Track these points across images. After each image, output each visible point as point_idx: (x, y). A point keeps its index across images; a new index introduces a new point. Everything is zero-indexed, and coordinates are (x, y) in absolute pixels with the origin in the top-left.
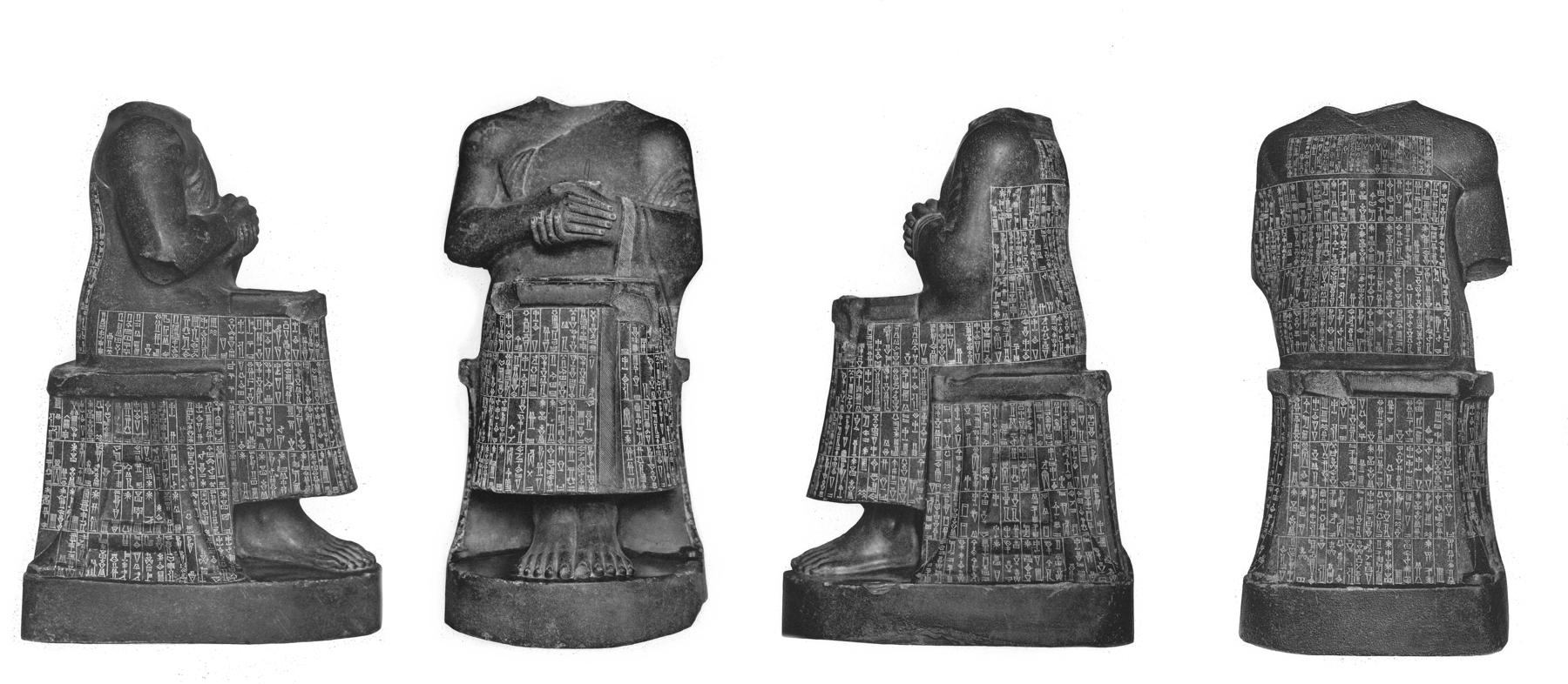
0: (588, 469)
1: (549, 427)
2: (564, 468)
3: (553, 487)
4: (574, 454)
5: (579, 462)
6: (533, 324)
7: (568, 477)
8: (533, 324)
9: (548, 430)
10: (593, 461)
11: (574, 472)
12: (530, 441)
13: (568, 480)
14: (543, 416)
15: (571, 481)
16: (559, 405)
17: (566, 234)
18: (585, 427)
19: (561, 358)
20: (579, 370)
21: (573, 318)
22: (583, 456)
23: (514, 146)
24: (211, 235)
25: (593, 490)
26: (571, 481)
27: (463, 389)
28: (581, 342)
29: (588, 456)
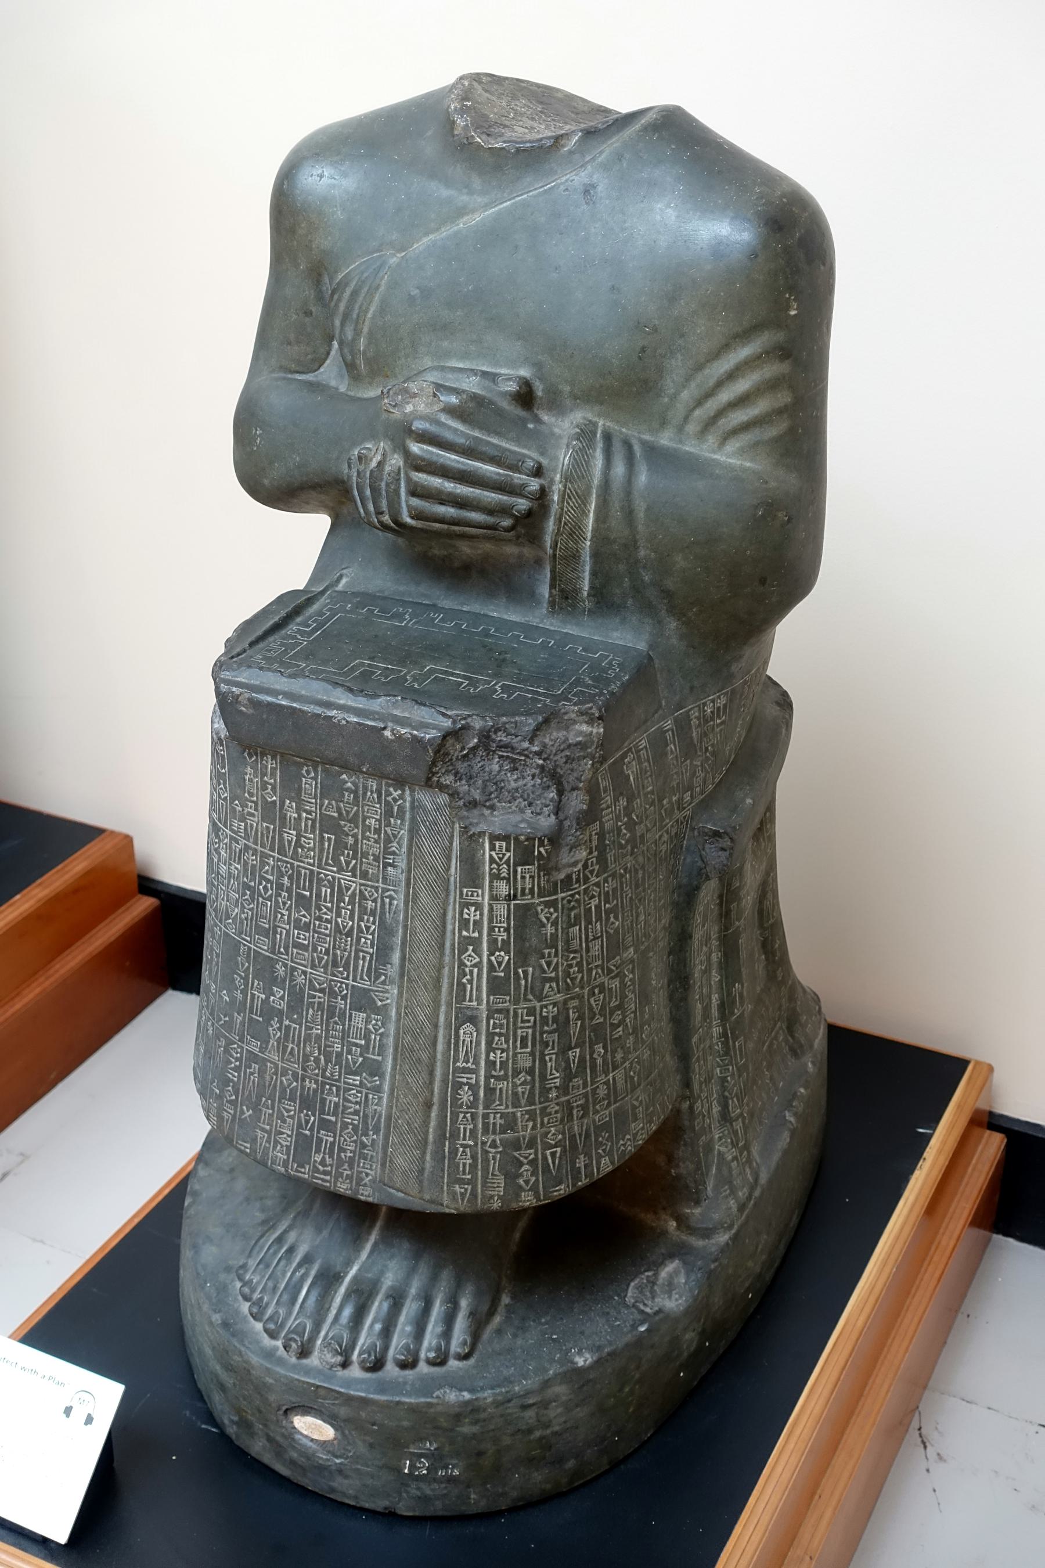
0: (364, 1146)
1: (288, 1028)
2: (311, 1130)
3: (286, 1163)
4: (337, 1105)
5: (345, 1126)
6: (264, 787)
7: (318, 1151)
8: (264, 787)
9: (287, 1035)
10: (377, 1131)
11: (333, 1144)
12: (255, 1046)
13: (318, 1158)
14: (279, 998)
15: (323, 1163)
16: (312, 987)
17: (556, 1048)
18: (365, 1049)
19: (320, 880)
20: (361, 919)
21: (349, 797)
22: (356, 1113)
23: (471, 756)
24: (796, 315)
25: (417, 1514)
26: (323, 1163)
27: (223, 650)
28: (365, 855)
29: (366, 1116)
